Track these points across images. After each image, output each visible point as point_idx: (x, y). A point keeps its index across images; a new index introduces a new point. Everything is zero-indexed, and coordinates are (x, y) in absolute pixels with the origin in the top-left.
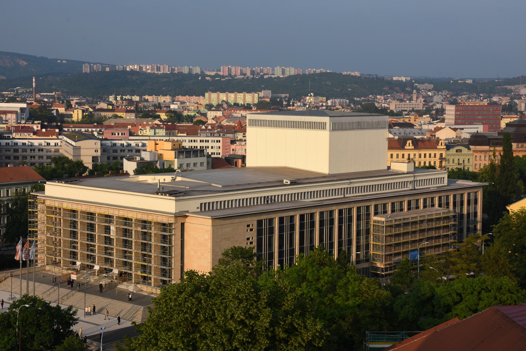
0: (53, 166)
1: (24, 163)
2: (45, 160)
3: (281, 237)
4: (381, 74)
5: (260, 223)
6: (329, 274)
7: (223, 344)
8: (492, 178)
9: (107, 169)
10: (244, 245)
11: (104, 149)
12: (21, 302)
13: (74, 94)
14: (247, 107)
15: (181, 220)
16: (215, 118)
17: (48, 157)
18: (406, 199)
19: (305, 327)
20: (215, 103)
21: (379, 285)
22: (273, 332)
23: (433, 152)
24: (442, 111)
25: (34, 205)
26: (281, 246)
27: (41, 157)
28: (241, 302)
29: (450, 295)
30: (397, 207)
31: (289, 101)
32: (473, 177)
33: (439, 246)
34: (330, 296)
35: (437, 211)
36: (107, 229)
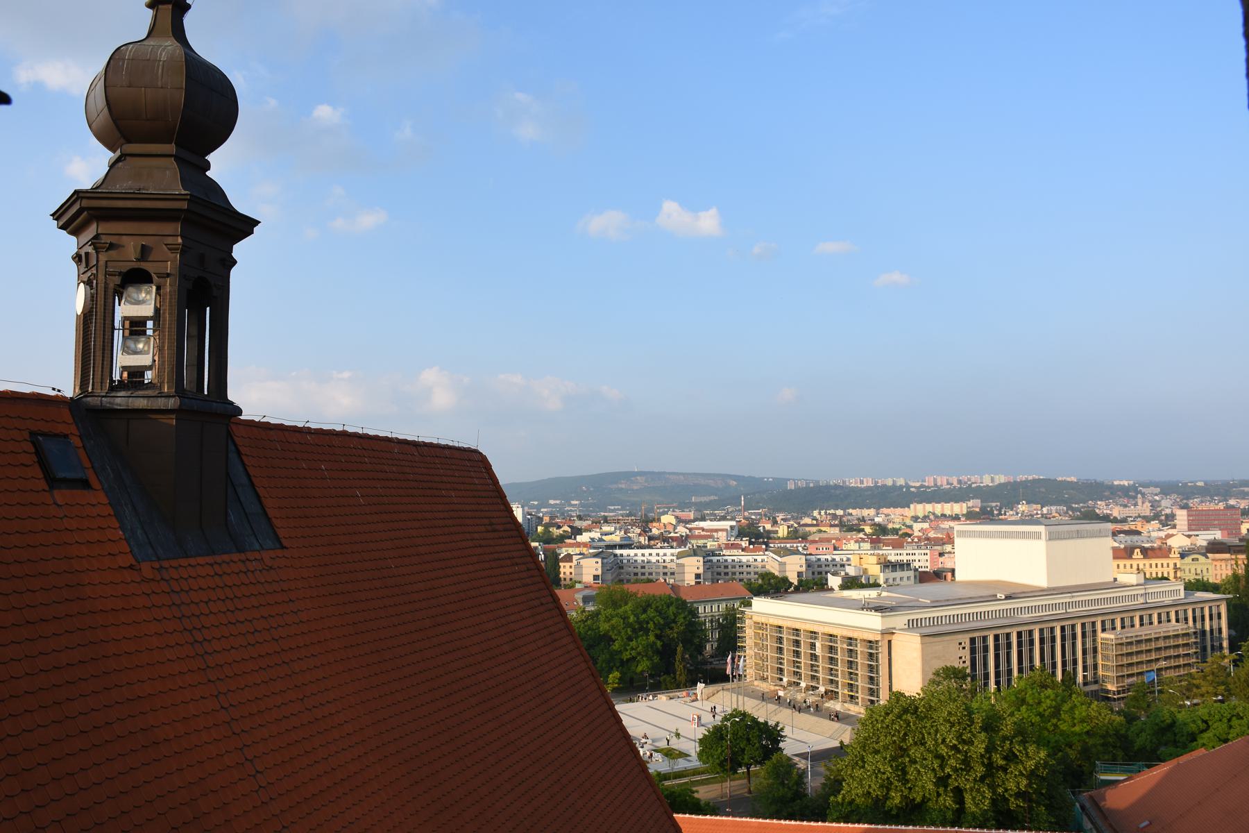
0: (760, 581)
1: (733, 579)
2: (753, 576)
3: (997, 656)
4: (1099, 479)
5: (973, 641)
6: (1052, 697)
7: (934, 770)
8: (1237, 590)
9: (813, 583)
10: (957, 664)
11: (809, 565)
12: (732, 716)
13: (780, 511)
14: (956, 518)
15: (888, 637)
16: (921, 530)
17: (756, 573)
18: (1138, 614)
19: (1027, 754)
20: (921, 515)
21: (1112, 710)
22: (990, 758)
23: (1165, 561)
24: (1171, 517)
25: (742, 620)
26: (997, 666)
27: (749, 573)
28: (953, 725)
29: (1194, 722)
30: (1127, 623)
31: (1000, 510)
32: (1215, 588)
33: (1179, 666)
34: (1054, 721)
35: (1174, 627)
36: (813, 646)
